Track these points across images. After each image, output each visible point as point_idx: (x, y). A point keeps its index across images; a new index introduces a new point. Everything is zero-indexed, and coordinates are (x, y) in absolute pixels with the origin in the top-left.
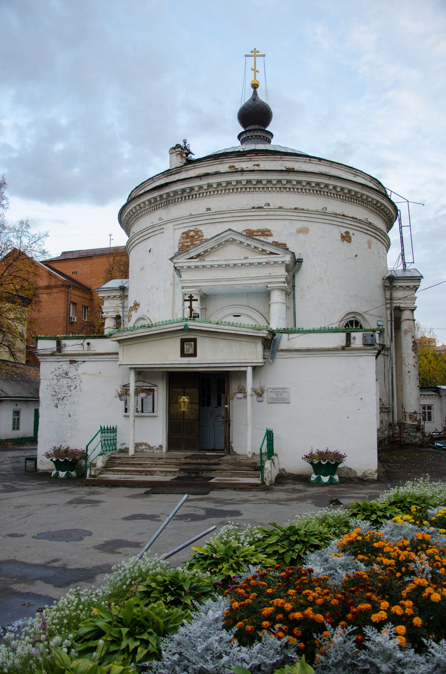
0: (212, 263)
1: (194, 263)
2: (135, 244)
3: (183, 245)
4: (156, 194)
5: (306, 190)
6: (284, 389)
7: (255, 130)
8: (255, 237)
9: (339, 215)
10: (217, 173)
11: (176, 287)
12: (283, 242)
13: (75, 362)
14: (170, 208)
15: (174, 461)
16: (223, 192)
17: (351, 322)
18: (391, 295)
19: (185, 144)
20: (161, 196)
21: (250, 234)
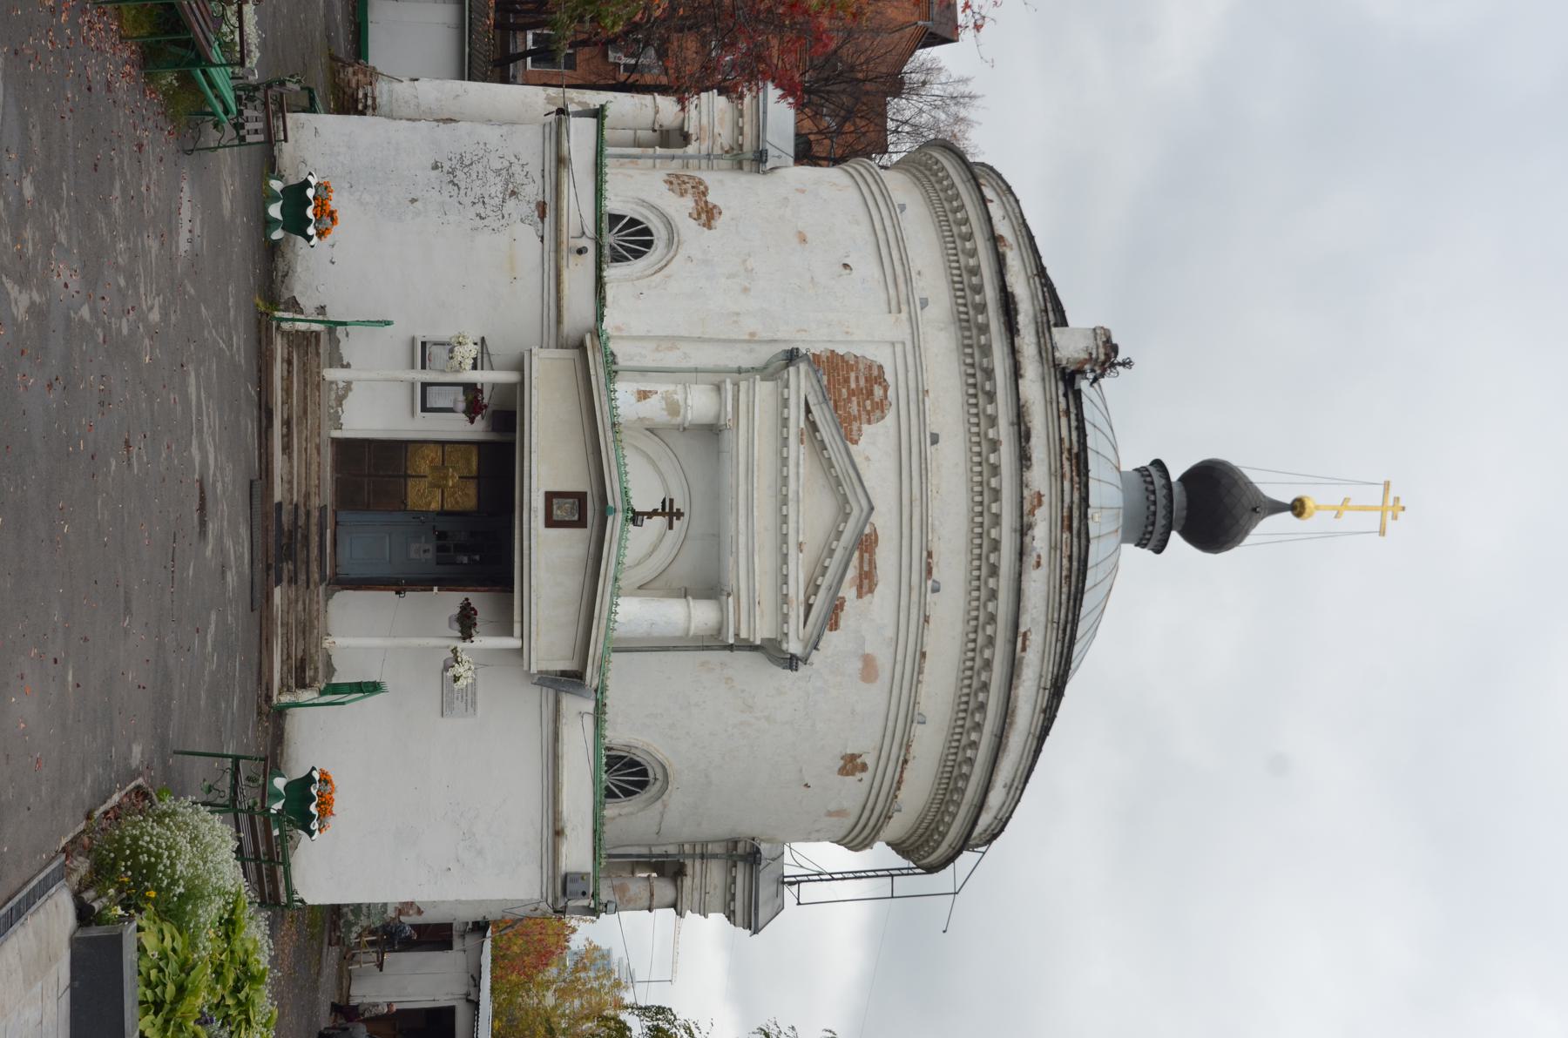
3: (850, 368)
4: (991, 294)
5: (971, 677)
6: (474, 703)
7: (1171, 501)
8: (856, 554)
10: (1024, 459)
12: (842, 623)
13: (542, 216)
14: (952, 328)
15: (314, 482)
16: (977, 479)
17: (644, 773)
18: (715, 856)
20: (982, 308)
21: (866, 544)
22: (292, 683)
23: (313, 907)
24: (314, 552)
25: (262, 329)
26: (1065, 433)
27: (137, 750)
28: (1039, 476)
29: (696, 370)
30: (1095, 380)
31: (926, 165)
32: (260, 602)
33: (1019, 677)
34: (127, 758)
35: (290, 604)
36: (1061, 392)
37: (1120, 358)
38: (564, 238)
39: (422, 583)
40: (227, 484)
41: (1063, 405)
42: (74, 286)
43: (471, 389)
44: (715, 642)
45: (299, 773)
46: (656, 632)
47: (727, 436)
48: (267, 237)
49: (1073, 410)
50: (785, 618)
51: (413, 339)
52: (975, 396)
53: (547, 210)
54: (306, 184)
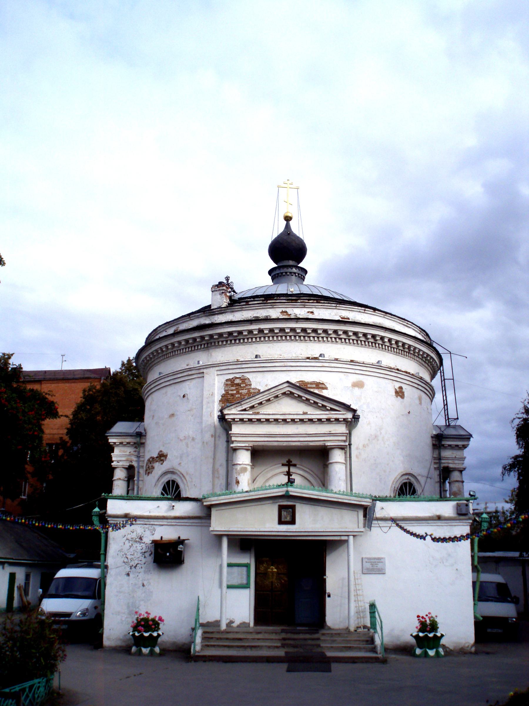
4: (196, 335)
6: (379, 559)
9: (393, 369)
10: (267, 320)
11: (217, 439)
14: (211, 351)
17: (405, 484)
19: (228, 282)
20: (202, 338)
28: (275, 313)
31: (145, 366)
37: (225, 282)
45: (413, 641)
50: (337, 420)
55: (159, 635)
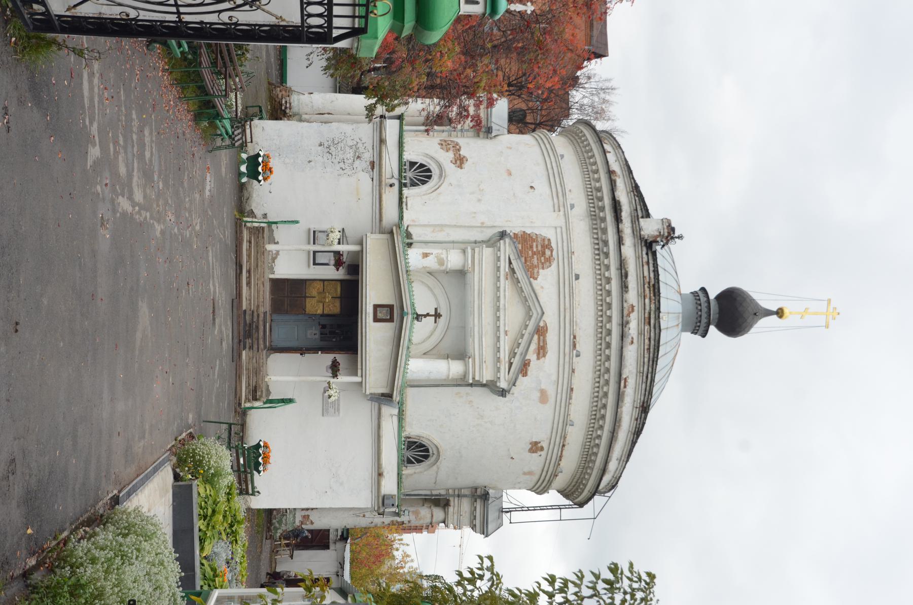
0: (502, 289)
1: (504, 266)
2: (547, 159)
3: (533, 240)
4: (607, 201)
6: (338, 410)
8: (536, 337)
10: (624, 287)
11: (479, 229)
12: (529, 373)
13: (373, 168)
14: (587, 220)
16: (599, 298)
17: (427, 450)
18: (465, 496)
20: (602, 209)
21: (541, 331)
22: (251, 397)
23: (259, 510)
24: (261, 334)
25: (238, 225)
26: (646, 274)
27: (191, 416)
28: (632, 296)
29: (453, 242)
30: (663, 246)
31: (576, 133)
32: (236, 357)
33: (623, 401)
34: (187, 419)
35: (250, 359)
36: (644, 253)
37: (676, 235)
38: (383, 178)
39: (314, 350)
40: (223, 299)
41: (645, 259)
42: (173, 220)
43: (338, 254)
44: (462, 382)
46: (432, 377)
47: (469, 276)
48: (239, 181)
49: (651, 262)
50: (498, 370)
51: (309, 230)
52: (599, 255)
53: (375, 165)
54: (258, 155)
55: (259, 181)
